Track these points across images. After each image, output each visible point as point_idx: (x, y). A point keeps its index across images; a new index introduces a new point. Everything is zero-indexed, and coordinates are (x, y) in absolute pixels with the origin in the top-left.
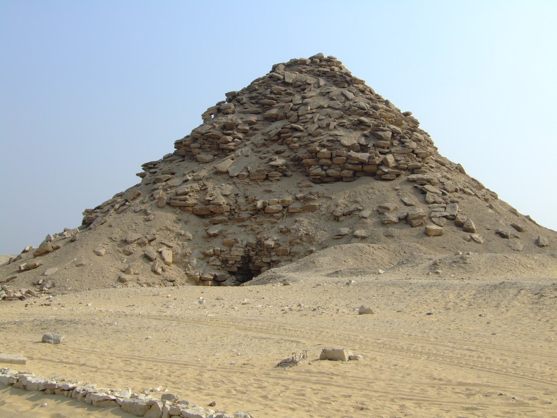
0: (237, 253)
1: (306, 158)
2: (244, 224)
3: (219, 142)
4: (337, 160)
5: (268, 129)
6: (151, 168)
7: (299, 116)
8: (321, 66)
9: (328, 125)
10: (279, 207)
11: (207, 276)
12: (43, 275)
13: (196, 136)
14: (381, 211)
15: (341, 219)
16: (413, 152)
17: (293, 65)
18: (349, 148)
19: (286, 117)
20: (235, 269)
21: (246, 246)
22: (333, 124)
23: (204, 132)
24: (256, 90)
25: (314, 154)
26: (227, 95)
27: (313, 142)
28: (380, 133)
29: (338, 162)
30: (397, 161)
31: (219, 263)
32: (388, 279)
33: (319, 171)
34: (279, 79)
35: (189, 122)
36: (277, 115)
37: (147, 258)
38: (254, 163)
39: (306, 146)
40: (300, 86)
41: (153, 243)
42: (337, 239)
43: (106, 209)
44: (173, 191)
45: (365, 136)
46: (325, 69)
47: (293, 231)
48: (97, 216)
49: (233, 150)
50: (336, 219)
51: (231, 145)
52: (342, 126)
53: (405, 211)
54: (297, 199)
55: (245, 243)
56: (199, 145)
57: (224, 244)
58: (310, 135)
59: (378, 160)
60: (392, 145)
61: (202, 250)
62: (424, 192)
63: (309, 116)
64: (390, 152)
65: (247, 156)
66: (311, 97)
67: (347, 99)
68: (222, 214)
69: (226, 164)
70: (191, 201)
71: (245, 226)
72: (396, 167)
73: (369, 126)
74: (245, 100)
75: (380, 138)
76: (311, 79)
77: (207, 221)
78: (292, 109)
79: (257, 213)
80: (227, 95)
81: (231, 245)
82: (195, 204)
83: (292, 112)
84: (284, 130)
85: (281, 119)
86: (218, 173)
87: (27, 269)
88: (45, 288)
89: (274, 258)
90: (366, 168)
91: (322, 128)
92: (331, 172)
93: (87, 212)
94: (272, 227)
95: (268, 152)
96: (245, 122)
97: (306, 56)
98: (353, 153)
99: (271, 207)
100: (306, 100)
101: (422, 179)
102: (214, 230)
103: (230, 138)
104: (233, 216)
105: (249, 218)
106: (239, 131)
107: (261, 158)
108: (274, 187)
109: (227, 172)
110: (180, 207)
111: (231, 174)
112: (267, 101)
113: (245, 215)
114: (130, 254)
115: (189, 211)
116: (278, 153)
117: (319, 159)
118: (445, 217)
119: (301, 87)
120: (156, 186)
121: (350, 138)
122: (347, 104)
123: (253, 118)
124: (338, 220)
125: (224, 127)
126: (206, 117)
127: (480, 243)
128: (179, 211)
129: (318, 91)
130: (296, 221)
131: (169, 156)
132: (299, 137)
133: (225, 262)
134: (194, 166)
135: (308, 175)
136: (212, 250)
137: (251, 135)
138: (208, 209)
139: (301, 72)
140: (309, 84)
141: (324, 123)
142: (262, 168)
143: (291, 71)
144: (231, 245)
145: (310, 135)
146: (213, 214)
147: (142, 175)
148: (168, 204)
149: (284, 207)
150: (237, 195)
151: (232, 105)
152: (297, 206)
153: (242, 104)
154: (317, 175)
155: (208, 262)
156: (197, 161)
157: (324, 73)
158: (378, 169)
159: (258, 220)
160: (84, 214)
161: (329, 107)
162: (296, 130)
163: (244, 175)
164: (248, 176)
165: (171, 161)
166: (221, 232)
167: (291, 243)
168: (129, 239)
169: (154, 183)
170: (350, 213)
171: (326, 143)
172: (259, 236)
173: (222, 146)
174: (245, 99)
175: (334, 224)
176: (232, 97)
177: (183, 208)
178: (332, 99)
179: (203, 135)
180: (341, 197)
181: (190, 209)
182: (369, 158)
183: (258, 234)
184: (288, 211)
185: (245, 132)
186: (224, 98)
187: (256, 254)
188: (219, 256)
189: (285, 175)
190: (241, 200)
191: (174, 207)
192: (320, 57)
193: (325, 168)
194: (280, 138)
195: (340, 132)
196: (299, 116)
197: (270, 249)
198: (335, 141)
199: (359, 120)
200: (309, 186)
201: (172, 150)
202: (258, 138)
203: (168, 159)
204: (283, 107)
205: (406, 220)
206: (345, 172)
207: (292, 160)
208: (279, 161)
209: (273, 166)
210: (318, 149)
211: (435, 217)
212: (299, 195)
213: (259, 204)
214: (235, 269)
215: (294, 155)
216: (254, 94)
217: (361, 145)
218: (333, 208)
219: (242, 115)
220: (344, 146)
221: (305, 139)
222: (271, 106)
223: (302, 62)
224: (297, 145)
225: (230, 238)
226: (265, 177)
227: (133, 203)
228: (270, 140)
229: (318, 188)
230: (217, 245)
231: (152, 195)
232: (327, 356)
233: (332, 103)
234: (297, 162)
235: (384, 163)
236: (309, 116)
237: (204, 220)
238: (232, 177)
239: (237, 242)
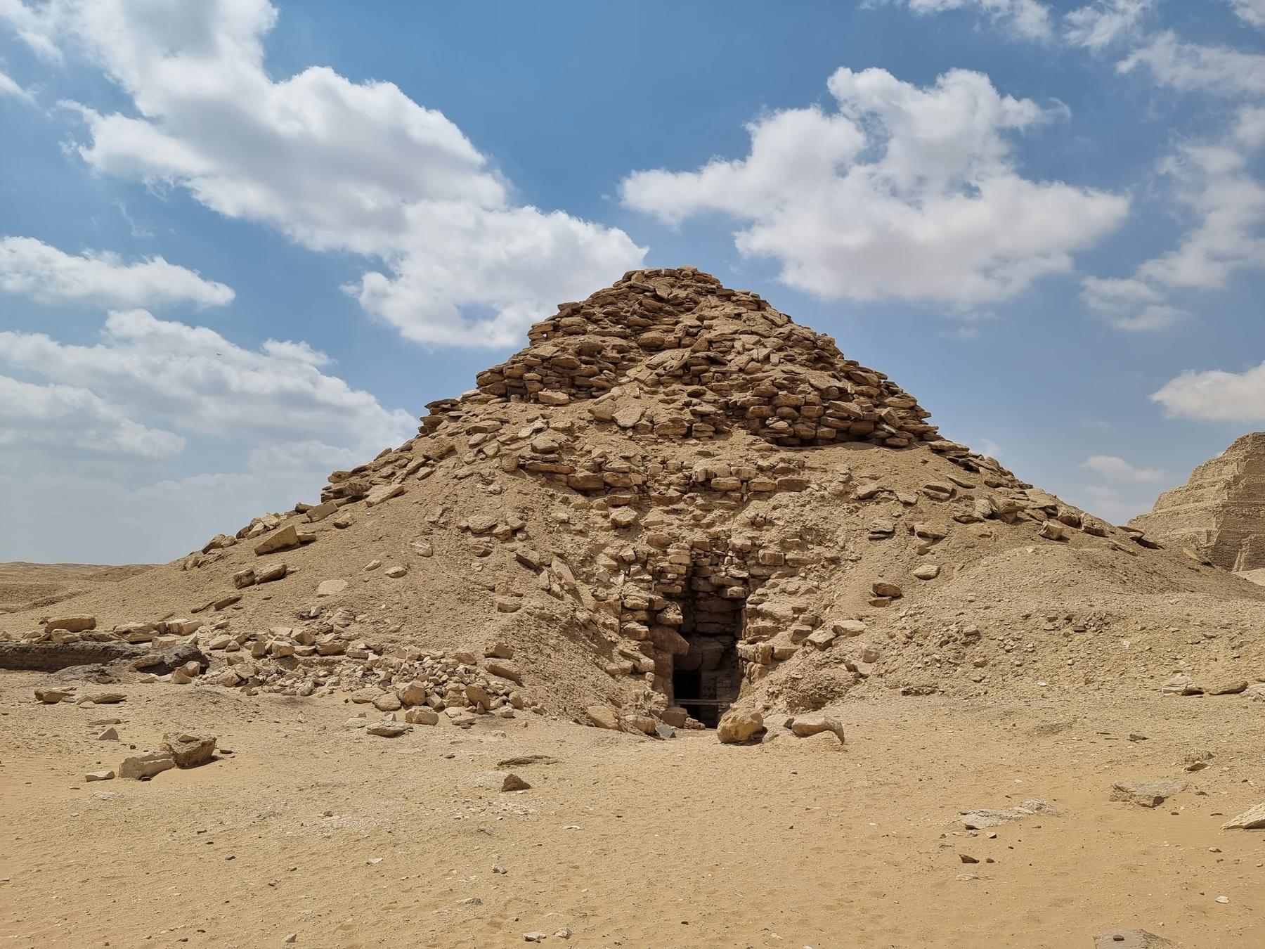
1: (753, 404)
2: (675, 506)
4: (805, 410)
21: (692, 547)
26: (561, 307)
29: (810, 414)
42: (877, 539)
56: (539, 377)
65: (925, 462)
66: (713, 318)
68: (627, 488)
71: (676, 511)
81: (663, 545)
89: (757, 571)
115: (561, 480)
133: (659, 574)
136: (631, 552)
138: (601, 479)
144: (663, 545)
149: (742, 482)
153: (596, 322)
156: (537, 401)
158: (876, 429)
174: (598, 311)
181: (564, 477)
186: (557, 312)
188: (644, 564)
194: (687, 373)
220: (817, 389)
221: (735, 376)
226: (684, 431)
232: (1134, 738)
234: (737, 413)
238: (624, 429)
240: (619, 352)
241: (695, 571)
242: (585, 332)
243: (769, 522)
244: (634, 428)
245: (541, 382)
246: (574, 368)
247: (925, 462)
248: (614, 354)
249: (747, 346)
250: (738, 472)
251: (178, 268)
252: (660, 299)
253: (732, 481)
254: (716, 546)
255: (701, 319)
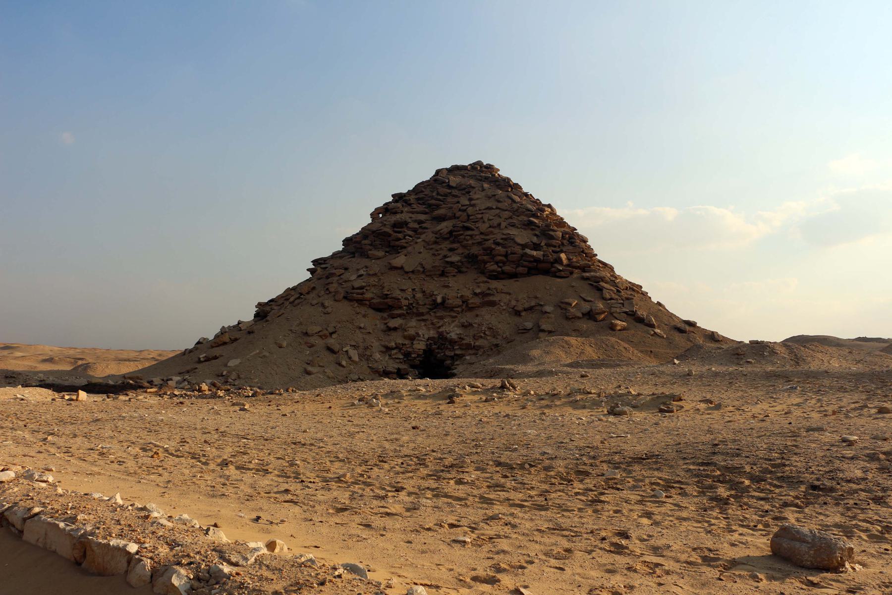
0: (419, 347)
2: (424, 318)
3: (390, 239)
4: (511, 257)
5: (439, 228)
6: (320, 264)
7: (469, 216)
8: (482, 172)
9: (499, 225)
10: (459, 302)
11: (390, 369)
12: (226, 365)
13: (365, 233)
14: (563, 306)
15: (523, 314)
16: (583, 252)
17: (455, 169)
18: (524, 246)
19: (454, 217)
20: (417, 362)
21: (428, 339)
22: (503, 224)
23: (374, 229)
24: (422, 192)
25: (489, 251)
26: (393, 196)
27: (487, 240)
28: (551, 233)
30: (569, 259)
31: (401, 357)
32: (660, 392)
33: (495, 267)
34: (444, 182)
35: (358, 221)
36: (446, 215)
37: (330, 350)
38: (427, 259)
39: (480, 243)
40: (465, 189)
41: (334, 336)
43: (280, 302)
44: (349, 284)
45: (536, 235)
46: (482, 174)
47: (475, 325)
48: (272, 309)
49: (405, 247)
50: (518, 313)
51: (403, 242)
52: (513, 225)
53: (586, 307)
54: (476, 294)
55: (426, 336)
57: (405, 337)
58: (482, 233)
59: (551, 257)
60: (563, 244)
61: (383, 343)
62: (600, 289)
63: (480, 216)
64: (562, 251)
65: (420, 253)
66: (478, 199)
67: (514, 201)
68: (400, 308)
69: (399, 260)
70: (368, 295)
71: (423, 320)
72: (568, 265)
73: (539, 227)
74: (412, 201)
75: (552, 237)
76: (472, 182)
77: (385, 315)
78: (460, 210)
79: (435, 308)
80: (393, 196)
81: (412, 338)
82: (372, 298)
83: (460, 213)
84: (456, 229)
85: (450, 218)
86: (393, 268)
87: (207, 359)
88: (230, 380)
89: (458, 352)
90: (541, 266)
91: (493, 227)
92: (507, 268)
93: (260, 305)
94: (453, 321)
95: (441, 249)
96: (415, 221)
97: (466, 162)
98: (528, 251)
99: (450, 301)
100: (473, 202)
101: (596, 277)
102: (393, 323)
103: (400, 236)
104: (412, 311)
105: (428, 313)
106: (409, 228)
107: (434, 255)
108: (451, 281)
109: (402, 268)
110: (358, 301)
111: (407, 269)
112: (433, 202)
113: (423, 310)
114: (312, 346)
116: (451, 250)
117: (494, 256)
118: (626, 313)
119: (466, 190)
120: (330, 280)
121: (522, 237)
122: (515, 205)
123: (422, 217)
124: (520, 315)
125: (395, 225)
126: (374, 215)
127: (663, 337)
128: (356, 305)
129: (483, 194)
130: (477, 316)
131: (339, 252)
132: (471, 236)
133: (407, 355)
134: (366, 262)
135: (483, 273)
137: (421, 234)
139: (463, 177)
140: (474, 188)
141: (495, 223)
142: (437, 264)
143: (455, 176)
144: (412, 338)
145: (482, 233)
146: (390, 308)
147: (311, 271)
148: (345, 298)
149: (463, 302)
150: (413, 290)
151: (399, 205)
152: (477, 301)
153: (410, 205)
154: (494, 271)
155: (390, 355)
156: (368, 257)
157: (486, 178)
159: (438, 314)
160: (256, 307)
161: (497, 208)
162: (468, 229)
163: (419, 271)
164: (423, 272)
165: (341, 257)
166: (401, 325)
167: (475, 338)
168: (310, 332)
169: (327, 277)
170: (530, 309)
171: (501, 241)
172: (440, 330)
173: (392, 243)
174: (412, 198)
175: (517, 319)
176: (398, 197)
177: (361, 302)
178: (499, 201)
179: (373, 232)
180: (519, 291)
181: (367, 303)
182: (544, 256)
183: (439, 327)
184: (467, 306)
185: (415, 230)
186: (391, 199)
187: (438, 348)
188: (400, 349)
189: (460, 272)
190: (419, 295)
191: (351, 300)
192: (479, 163)
193: (501, 265)
194: (452, 236)
195: (513, 232)
196: (469, 216)
197: (452, 342)
198: (509, 239)
199: (529, 220)
200: (486, 282)
201: (340, 247)
202: (429, 236)
203: (335, 255)
204: (451, 208)
205: (590, 315)
206: (520, 269)
207: (465, 257)
208: (455, 258)
209: (447, 262)
210: (493, 246)
211: (616, 312)
212: (478, 291)
213: (439, 300)
214: (417, 362)
215: (467, 252)
216: (421, 195)
217: (534, 244)
218: (513, 303)
219: (411, 215)
220: (519, 244)
221: (477, 237)
222: (438, 207)
223: (463, 168)
224: (470, 242)
225: (412, 332)
226: (440, 272)
227: (307, 296)
228: (440, 238)
229: (495, 284)
230: (397, 339)
231: (327, 289)
233: (500, 205)
234: (472, 259)
235: (560, 261)
236: (480, 216)
237: (382, 314)
238: (407, 273)
239: (418, 334)
240: (419, 223)
241: (428, 352)
242: (402, 212)
243: (470, 325)
244: (413, 272)
245: (371, 245)
246: (390, 235)
247: (420, 253)
248: (416, 226)
249: (491, 218)
250: (462, 296)
251: (357, 230)
252: (450, 187)
253: (459, 302)
254: (442, 340)
255: (470, 200)
